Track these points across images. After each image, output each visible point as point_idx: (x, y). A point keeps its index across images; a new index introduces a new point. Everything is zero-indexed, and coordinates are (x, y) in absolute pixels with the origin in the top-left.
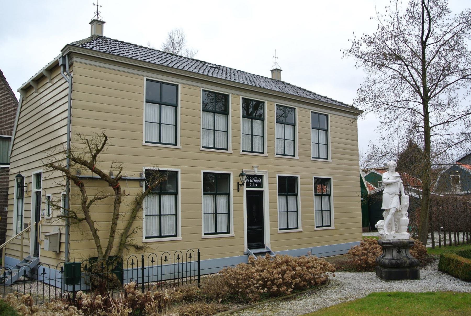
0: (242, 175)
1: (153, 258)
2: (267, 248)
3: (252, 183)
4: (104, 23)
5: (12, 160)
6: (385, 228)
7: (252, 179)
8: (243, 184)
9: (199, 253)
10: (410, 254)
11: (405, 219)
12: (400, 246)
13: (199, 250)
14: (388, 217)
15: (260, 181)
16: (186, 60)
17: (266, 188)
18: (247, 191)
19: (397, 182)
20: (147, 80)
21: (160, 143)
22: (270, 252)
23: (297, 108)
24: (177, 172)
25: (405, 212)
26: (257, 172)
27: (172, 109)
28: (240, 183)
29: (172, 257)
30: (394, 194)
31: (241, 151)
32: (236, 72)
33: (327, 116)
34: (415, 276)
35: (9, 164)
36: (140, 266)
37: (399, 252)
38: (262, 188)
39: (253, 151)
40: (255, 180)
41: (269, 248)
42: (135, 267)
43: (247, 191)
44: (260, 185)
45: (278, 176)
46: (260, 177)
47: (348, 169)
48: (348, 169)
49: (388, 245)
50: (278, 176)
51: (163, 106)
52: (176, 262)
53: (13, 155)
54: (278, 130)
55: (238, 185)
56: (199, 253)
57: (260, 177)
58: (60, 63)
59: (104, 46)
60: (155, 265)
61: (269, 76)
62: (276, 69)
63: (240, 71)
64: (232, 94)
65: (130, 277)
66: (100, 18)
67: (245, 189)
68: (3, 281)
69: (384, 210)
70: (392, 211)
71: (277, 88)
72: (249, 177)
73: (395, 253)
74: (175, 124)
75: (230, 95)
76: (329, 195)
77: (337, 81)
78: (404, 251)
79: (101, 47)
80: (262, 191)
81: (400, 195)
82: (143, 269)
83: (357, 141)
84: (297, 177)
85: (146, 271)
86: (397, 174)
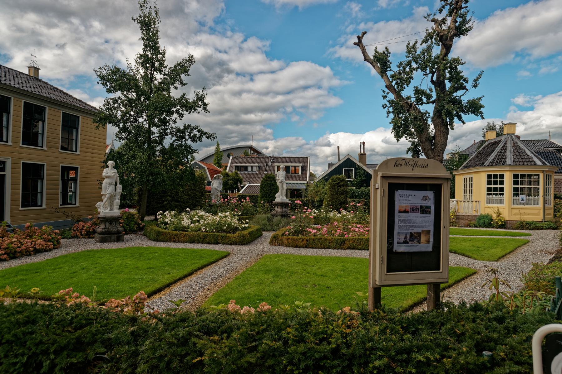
6: (102, 208)
25: (118, 197)
32: (14, 73)
34: (119, 239)
37: (111, 224)
38: (4, 171)
47: (89, 161)
48: (89, 161)
59: (26, 79)
61: (26, 71)
62: (34, 67)
63: (12, 69)
68: (425, 100)
69: (103, 195)
70: (107, 196)
80: (4, 175)
81: (116, 185)
83: (106, 139)
84: (44, 165)
86: (115, 170)
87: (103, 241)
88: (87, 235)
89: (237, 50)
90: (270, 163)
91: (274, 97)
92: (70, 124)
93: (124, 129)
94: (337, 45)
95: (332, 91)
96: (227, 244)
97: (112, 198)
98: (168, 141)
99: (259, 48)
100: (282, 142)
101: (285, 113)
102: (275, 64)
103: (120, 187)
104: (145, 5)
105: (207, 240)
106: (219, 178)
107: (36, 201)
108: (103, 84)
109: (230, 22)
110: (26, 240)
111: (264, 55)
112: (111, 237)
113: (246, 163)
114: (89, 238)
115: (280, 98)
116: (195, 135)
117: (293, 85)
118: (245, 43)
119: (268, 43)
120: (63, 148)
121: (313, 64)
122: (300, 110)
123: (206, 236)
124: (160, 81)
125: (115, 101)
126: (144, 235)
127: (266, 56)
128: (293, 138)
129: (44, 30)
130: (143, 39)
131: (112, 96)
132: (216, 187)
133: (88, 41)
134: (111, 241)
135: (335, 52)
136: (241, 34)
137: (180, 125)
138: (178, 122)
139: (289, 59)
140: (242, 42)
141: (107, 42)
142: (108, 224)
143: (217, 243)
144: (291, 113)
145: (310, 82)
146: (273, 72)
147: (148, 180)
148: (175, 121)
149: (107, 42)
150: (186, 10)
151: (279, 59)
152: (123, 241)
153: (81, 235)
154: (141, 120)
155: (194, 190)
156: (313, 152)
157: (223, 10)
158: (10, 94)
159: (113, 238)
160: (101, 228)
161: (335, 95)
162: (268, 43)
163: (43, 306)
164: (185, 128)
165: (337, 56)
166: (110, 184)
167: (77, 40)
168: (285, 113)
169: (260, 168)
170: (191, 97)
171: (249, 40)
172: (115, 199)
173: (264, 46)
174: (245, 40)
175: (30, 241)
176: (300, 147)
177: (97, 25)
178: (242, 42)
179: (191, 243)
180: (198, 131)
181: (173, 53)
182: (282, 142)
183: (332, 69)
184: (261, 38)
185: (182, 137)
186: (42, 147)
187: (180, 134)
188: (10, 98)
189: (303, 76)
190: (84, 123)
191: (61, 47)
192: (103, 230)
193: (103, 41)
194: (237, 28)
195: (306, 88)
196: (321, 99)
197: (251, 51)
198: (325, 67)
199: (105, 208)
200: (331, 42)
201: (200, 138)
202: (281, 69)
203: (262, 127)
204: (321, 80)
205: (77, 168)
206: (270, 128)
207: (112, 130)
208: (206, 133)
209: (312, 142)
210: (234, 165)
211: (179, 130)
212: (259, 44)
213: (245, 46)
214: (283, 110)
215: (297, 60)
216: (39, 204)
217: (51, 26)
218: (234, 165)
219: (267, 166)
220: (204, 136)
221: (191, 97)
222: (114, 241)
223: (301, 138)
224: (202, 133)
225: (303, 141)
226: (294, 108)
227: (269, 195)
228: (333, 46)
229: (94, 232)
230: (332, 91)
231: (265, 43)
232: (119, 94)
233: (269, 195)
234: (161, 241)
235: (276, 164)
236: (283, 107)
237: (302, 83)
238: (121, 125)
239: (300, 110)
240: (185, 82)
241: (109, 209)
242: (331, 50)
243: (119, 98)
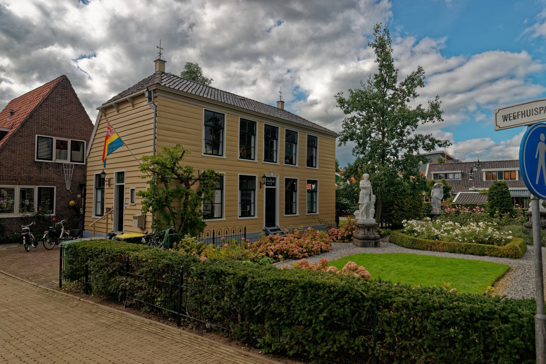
0: (264, 177)
2: (277, 227)
6: (360, 215)
11: (372, 210)
12: (368, 227)
14: (362, 208)
15: (274, 182)
16: (182, 80)
17: (277, 187)
20: (205, 110)
22: (279, 230)
24: (255, 177)
26: (272, 175)
29: (223, 231)
34: (376, 245)
36: (212, 237)
37: (368, 230)
40: (271, 181)
41: (279, 226)
44: (274, 184)
46: (274, 179)
53: (90, 156)
56: (214, 233)
57: (274, 179)
65: (218, 242)
66: (162, 58)
67: (265, 187)
70: (365, 205)
71: (192, 88)
72: (268, 178)
75: (226, 115)
80: (275, 189)
81: (370, 195)
82: (214, 238)
84: (255, 177)
85: (215, 240)
87: (364, 246)
88: (342, 239)
89: (408, 54)
90: (475, 169)
91: (451, 98)
92: (312, 143)
94: (535, 22)
95: (531, 79)
96: (496, 256)
99: (433, 48)
100: (463, 146)
101: (467, 112)
102: (453, 61)
103: (374, 197)
104: (379, 29)
105: (470, 251)
106: (439, 187)
107: (250, 212)
108: (341, 107)
109: (399, 29)
111: (439, 54)
112: (370, 243)
113: (446, 170)
114: (344, 242)
115: (460, 97)
117: (477, 80)
118: (417, 46)
119: (443, 40)
120: (308, 165)
121: (503, 52)
122: (486, 107)
123: (469, 247)
124: (391, 96)
125: (352, 120)
126: (390, 242)
127: (442, 54)
128: (478, 140)
129: (244, 72)
130: (378, 60)
132: (437, 196)
133: (273, 75)
134: (370, 247)
135: (534, 32)
136: (412, 38)
137: (412, 136)
138: (411, 134)
139: (469, 53)
140: (414, 46)
141: (289, 71)
142: (366, 230)
143: (484, 255)
144: (474, 112)
145: (498, 74)
146: (450, 70)
147: (389, 190)
149: (289, 71)
150: (353, 28)
151: (457, 55)
152: (379, 247)
153: (337, 239)
156: (506, 154)
157: (390, 19)
159: (371, 244)
160: (361, 233)
161: (535, 83)
162: (443, 40)
165: (536, 35)
166: (366, 194)
167: (266, 75)
168: (467, 112)
169: (463, 175)
170: (426, 107)
171: (420, 42)
172: (370, 208)
173: (438, 45)
174: (417, 43)
176: (488, 149)
177: (278, 59)
178: (414, 46)
179: (451, 252)
180: (430, 140)
181: (404, 70)
182: (463, 146)
183: (529, 52)
184: (435, 37)
187: (415, 143)
189: (490, 68)
190: (321, 141)
191: (254, 83)
192: (364, 236)
193: (286, 71)
194: (407, 33)
195: (492, 81)
196: (516, 90)
197: (424, 53)
198: (519, 52)
200: (526, 21)
202: (460, 65)
203: (440, 131)
204: (516, 68)
205: (317, 181)
206: (450, 132)
208: (439, 141)
209: (502, 142)
210: (433, 173)
212: (433, 43)
213: (417, 49)
214: (465, 110)
215: (480, 52)
216: (252, 214)
217: (248, 68)
218: (433, 173)
219: (471, 172)
220: (436, 144)
221: (426, 107)
222: (373, 247)
223: (488, 139)
225: (492, 142)
226: (478, 106)
227: (501, 204)
228: (530, 25)
230: (531, 79)
231: (439, 42)
232: (354, 114)
233: (501, 204)
234: (417, 249)
235: (483, 170)
236: (465, 107)
237: (488, 76)
239: (486, 107)
240: (417, 94)
241: (365, 217)
242: (527, 30)
243: (355, 117)
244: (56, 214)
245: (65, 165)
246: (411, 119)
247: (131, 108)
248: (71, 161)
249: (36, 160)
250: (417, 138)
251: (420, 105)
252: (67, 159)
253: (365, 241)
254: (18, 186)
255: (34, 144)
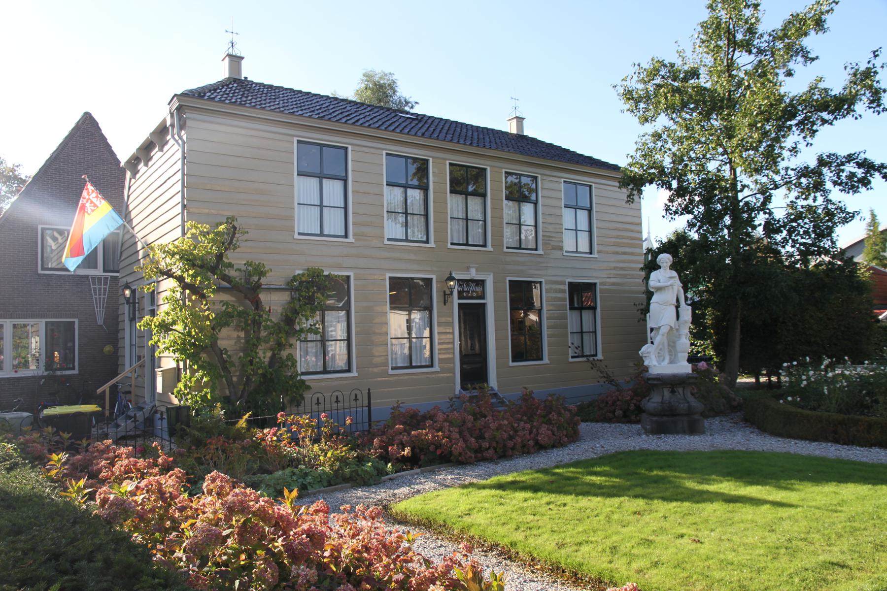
1: (356, 396)
3: (468, 292)
4: (243, 58)
5: (122, 265)
6: (653, 357)
7: (468, 285)
8: (452, 293)
9: (369, 394)
10: (690, 395)
13: (369, 390)
17: (490, 301)
18: (459, 304)
19: (672, 285)
20: (451, 164)
21: (322, 234)
23: (539, 176)
26: (473, 274)
27: (339, 185)
28: (448, 292)
30: (665, 304)
31: (296, 233)
33: (590, 186)
34: (693, 429)
35: (118, 272)
36: (366, 402)
39: (326, 233)
40: (473, 287)
41: (496, 388)
42: (359, 403)
43: (459, 304)
45: (510, 281)
46: (481, 283)
48: (623, 237)
49: (655, 382)
50: (510, 281)
51: (324, 181)
52: (353, 403)
53: (123, 258)
54: (454, 204)
55: (445, 295)
56: (369, 394)
57: (481, 283)
58: (168, 124)
60: (340, 405)
64: (352, 145)
70: (664, 330)
73: (667, 393)
74: (343, 205)
75: (431, 160)
76: (594, 308)
77: (614, 136)
78: (680, 390)
79: (254, 101)
80: (484, 305)
86: (674, 274)
87: (660, 429)
93: (681, 192)
97: (673, 334)
98: (780, 204)
110: (522, 424)
116: (852, 175)
125: (657, 136)
131: (649, 128)
134: (677, 433)
137: (808, 158)
138: (802, 151)
148: (794, 150)
154: (712, 166)
155: (608, 519)
158: (482, 162)
160: (654, 402)
163: (184, 542)
164: (822, 162)
175: (528, 426)
180: (859, 165)
185: (818, 186)
186: (536, 249)
187: (812, 179)
188: (485, 169)
199: (660, 357)
201: (865, 182)
207: (654, 198)
211: (805, 172)
222: (684, 433)
224: (868, 166)
229: (639, 410)
238: (674, 184)
241: (667, 361)
244: (79, 371)
245: (93, 278)
246: (787, 115)
247: (160, 154)
248: (105, 271)
249: (40, 272)
250: (822, 162)
251: (821, 80)
252: (96, 267)
253: (665, 419)
254: (8, 320)
255: (36, 243)
